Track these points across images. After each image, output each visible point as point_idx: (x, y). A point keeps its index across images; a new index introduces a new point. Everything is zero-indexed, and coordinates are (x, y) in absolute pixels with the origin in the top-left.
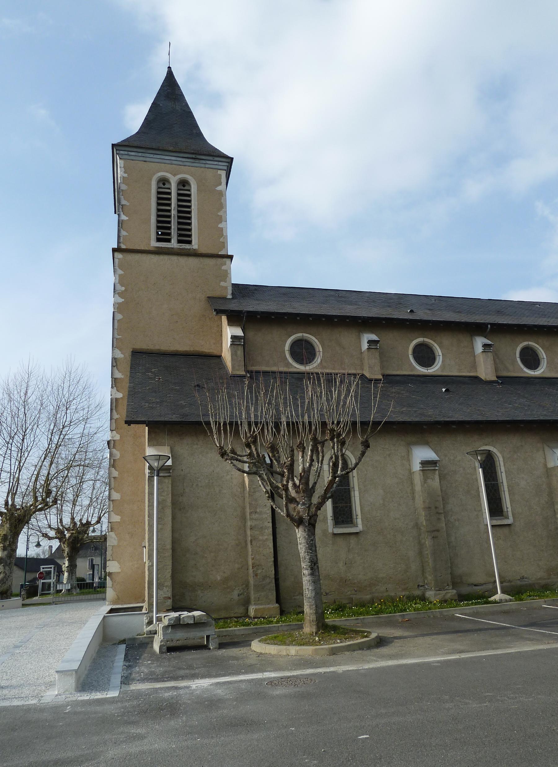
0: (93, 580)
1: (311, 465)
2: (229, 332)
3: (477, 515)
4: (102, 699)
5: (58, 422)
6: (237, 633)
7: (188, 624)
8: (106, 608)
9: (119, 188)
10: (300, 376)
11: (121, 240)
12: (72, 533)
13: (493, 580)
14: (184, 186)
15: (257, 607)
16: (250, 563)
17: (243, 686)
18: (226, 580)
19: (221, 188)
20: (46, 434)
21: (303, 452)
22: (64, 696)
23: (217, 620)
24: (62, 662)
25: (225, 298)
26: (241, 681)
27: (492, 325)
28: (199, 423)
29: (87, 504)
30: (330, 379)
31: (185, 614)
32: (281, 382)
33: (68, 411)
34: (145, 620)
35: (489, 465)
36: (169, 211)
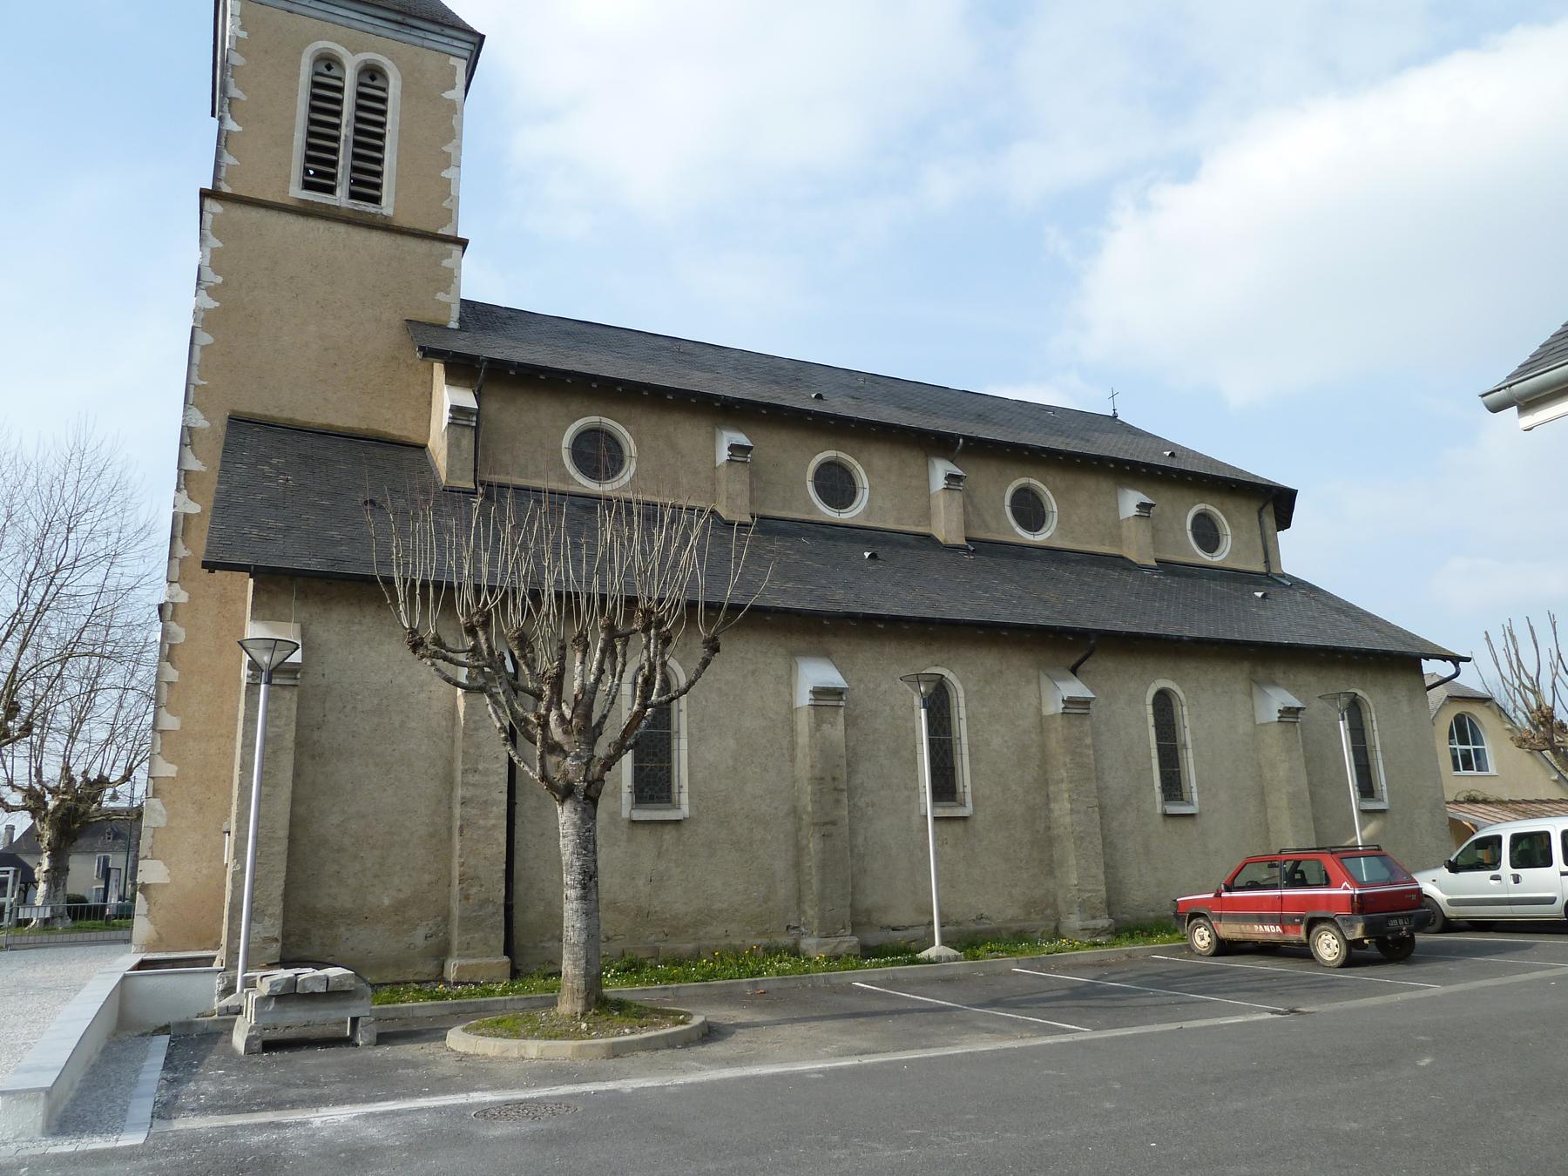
0: (105, 900)
1: (598, 680)
2: (448, 397)
3: (909, 797)
4: (105, 1150)
5: (46, 556)
6: (418, 1013)
7: (313, 993)
8: (129, 959)
9: (225, 61)
10: (587, 502)
11: (223, 174)
12: (63, 800)
13: (926, 921)
14: (373, 78)
15: (463, 962)
16: (456, 872)
17: (424, 1120)
18: (400, 907)
19: (455, 94)
20: (16, 581)
21: (584, 653)
22: (13, 1147)
23: (376, 987)
24: (16, 1072)
25: (443, 327)
26: (421, 1110)
27: (967, 439)
28: (369, 580)
29: (101, 737)
30: (651, 514)
31: (308, 972)
32: (552, 511)
33: (72, 536)
34: (218, 984)
35: (939, 705)
36: (337, 127)
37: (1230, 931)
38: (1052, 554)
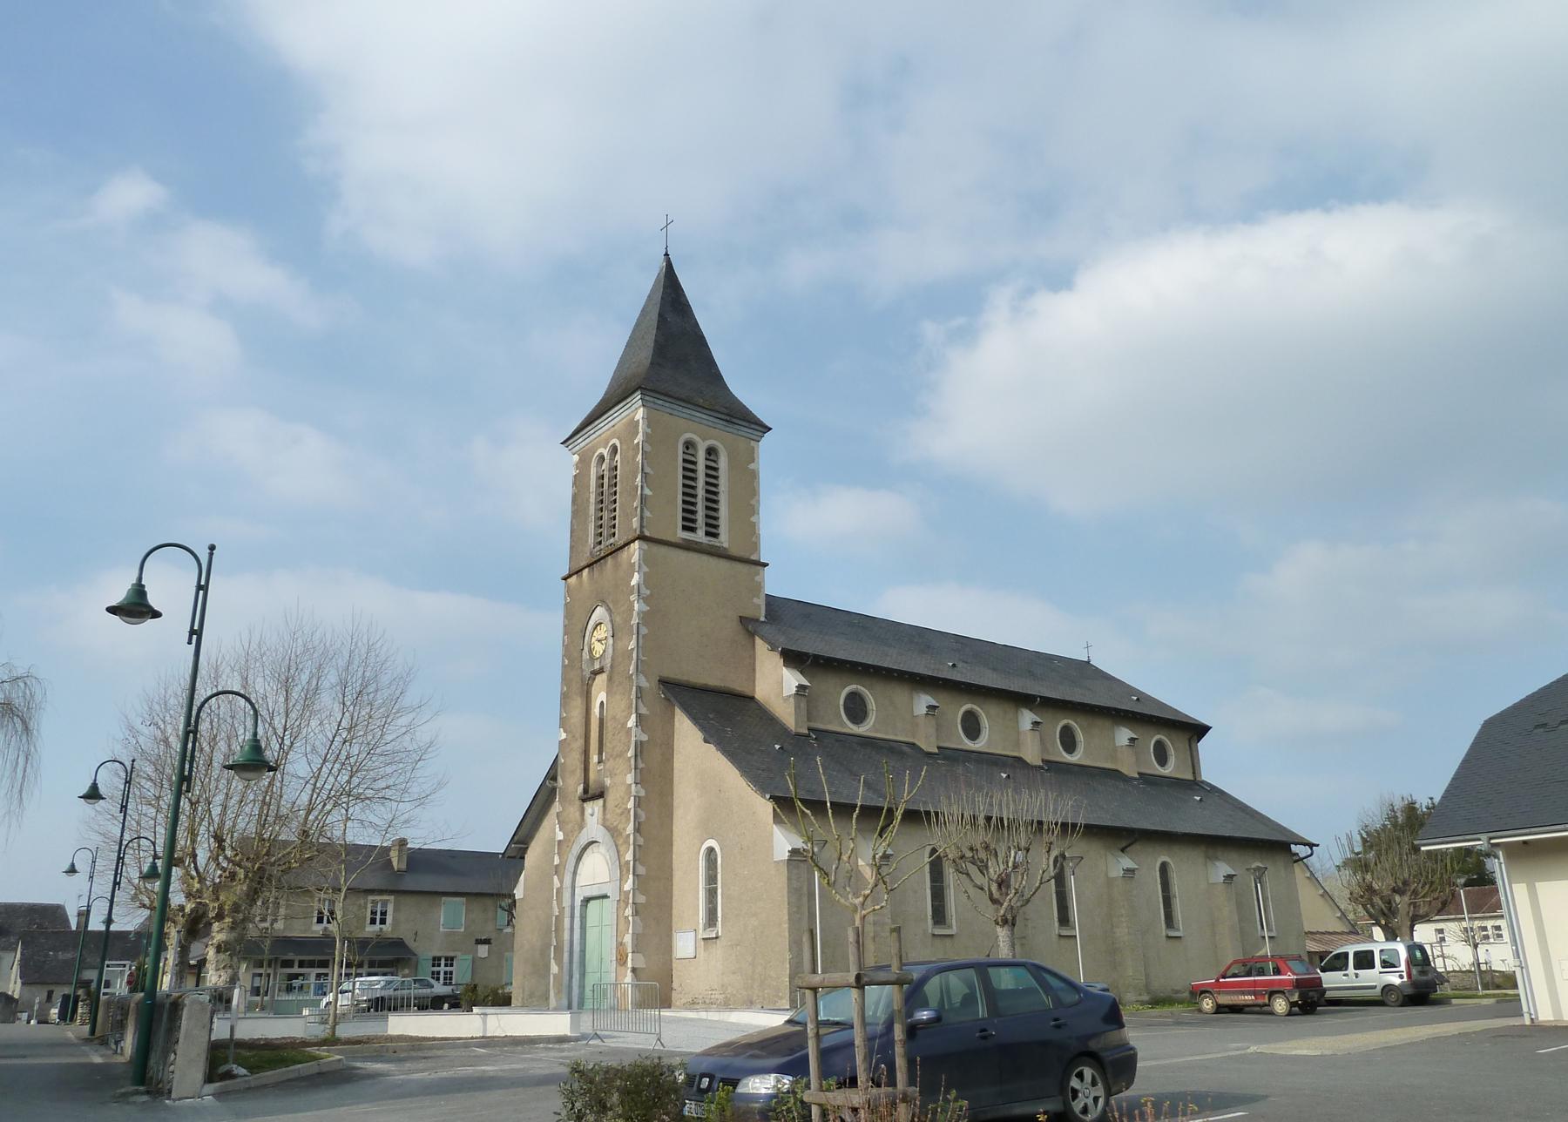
37: (1224, 1000)
38: (868, 742)
